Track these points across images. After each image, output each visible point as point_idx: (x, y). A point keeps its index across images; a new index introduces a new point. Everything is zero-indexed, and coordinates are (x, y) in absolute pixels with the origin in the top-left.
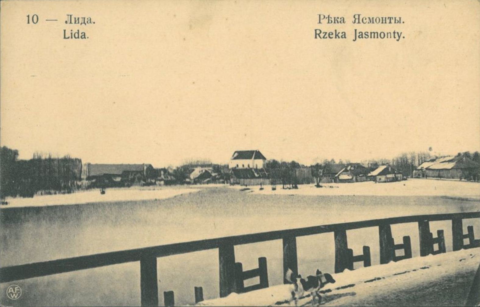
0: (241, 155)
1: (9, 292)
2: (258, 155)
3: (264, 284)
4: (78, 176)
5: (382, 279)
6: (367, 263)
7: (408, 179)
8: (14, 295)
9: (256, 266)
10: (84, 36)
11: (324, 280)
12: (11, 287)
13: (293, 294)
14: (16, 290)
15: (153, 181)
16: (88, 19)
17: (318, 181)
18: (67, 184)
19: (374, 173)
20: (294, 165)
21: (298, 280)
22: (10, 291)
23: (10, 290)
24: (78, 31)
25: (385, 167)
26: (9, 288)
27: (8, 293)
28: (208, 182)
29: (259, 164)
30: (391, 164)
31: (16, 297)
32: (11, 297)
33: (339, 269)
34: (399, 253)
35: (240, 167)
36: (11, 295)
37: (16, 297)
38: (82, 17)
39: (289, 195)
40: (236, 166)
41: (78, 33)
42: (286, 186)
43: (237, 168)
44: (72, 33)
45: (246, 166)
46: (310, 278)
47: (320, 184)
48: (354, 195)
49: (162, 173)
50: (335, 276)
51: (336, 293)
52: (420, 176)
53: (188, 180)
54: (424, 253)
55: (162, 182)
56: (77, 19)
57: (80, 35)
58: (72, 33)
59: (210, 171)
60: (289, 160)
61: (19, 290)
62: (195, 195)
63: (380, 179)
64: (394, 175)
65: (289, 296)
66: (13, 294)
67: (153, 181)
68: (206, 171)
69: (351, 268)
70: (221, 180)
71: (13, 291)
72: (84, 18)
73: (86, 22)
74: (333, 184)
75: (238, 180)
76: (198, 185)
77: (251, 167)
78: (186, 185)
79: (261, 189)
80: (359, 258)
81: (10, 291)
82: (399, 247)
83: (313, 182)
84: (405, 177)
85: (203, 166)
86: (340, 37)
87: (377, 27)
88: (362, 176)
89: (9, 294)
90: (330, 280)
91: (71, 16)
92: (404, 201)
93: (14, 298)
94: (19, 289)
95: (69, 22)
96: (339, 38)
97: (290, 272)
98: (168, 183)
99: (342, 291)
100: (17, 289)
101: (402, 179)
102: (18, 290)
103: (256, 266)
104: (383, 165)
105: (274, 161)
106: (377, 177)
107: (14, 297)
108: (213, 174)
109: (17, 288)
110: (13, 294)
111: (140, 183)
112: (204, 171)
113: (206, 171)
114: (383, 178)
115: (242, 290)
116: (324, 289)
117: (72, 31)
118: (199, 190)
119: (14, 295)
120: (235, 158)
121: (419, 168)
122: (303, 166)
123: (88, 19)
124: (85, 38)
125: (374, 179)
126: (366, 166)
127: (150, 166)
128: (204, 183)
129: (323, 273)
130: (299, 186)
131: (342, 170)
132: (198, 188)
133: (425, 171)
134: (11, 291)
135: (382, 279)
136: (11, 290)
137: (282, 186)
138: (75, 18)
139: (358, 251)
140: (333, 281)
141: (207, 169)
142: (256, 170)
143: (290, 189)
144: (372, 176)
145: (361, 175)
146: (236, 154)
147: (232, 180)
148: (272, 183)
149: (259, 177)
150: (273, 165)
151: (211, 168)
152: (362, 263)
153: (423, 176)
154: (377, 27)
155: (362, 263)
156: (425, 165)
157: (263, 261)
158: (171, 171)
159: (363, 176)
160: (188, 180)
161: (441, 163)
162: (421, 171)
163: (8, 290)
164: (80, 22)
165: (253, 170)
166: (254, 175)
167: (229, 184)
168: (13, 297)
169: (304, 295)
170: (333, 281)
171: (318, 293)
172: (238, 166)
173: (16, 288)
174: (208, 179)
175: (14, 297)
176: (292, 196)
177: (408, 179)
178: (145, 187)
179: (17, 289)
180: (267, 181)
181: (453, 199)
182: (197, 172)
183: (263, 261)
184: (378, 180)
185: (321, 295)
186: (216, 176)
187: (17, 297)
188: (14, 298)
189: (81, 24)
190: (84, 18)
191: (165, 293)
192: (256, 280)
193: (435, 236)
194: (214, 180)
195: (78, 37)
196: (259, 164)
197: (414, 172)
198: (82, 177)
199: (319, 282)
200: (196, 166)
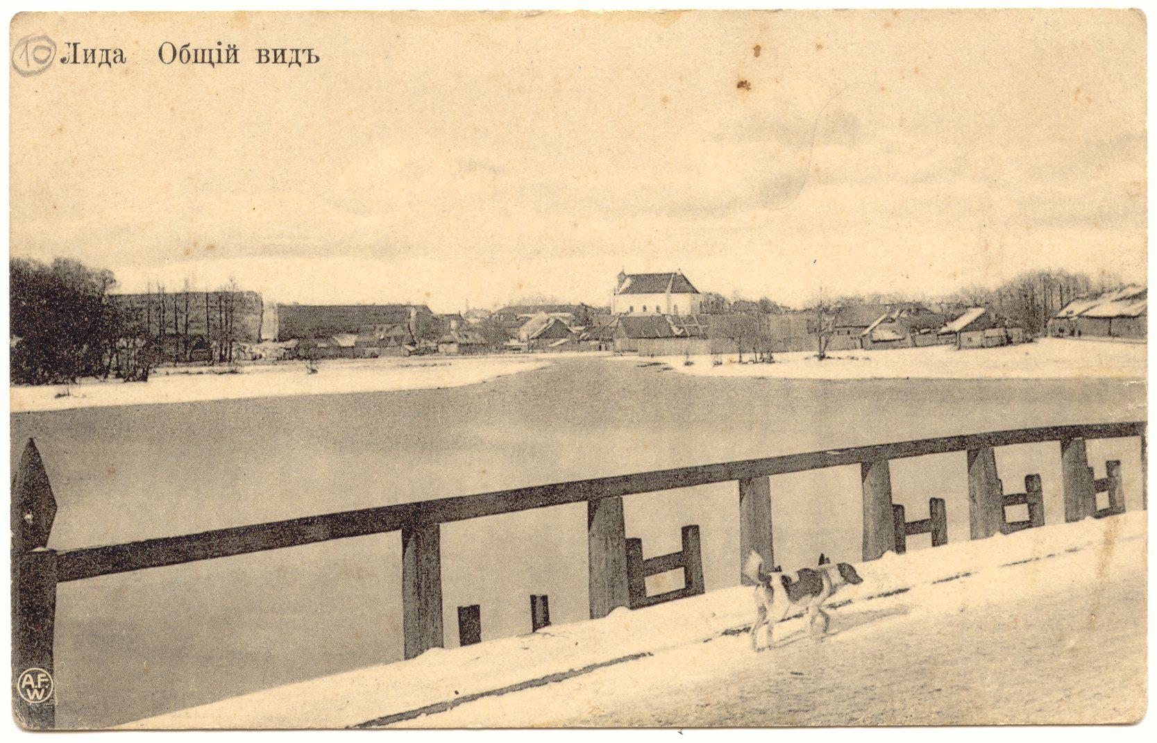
0: (643, 283)
1: (23, 686)
2: (680, 284)
3: (692, 588)
4: (254, 332)
6: (939, 540)
7: (1035, 340)
8: (36, 692)
9: (675, 546)
11: (836, 577)
12: (28, 673)
13: (763, 610)
14: (40, 680)
15: (432, 345)
17: (823, 346)
18: (228, 355)
19: (957, 325)
20: (766, 307)
21: (776, 580)
22: (25, 683)
23: (25, 679)
25: (980, 311)
26: (24, 676)
27: (21, 688)
28: (562, 348)
29: (683, 304)
30: (996, 304)
31: (39, 697)
32: (27, 697)
33: (871, 552)
34: (1017, 513)
35: (638, 311)
36: (28, 691)
37: (39, 697)
38: (103, 48)
39: (755, 378)
40: (629, 310)
42: (746, 357)
43: (631, 315)
45: (652, 311)
46: (803, 572)
47: (828, 354)
48: (908, 378)
49: (454, 324)
50: (861, 568)
51: (865, 609)
52: (1065, 334)
53: (514, 343)
54: (1072, 517)
55: (454, 348)
56: (89, 52)
59: (565, 322)
60: (753, 294)
61: (46, 680)
63: (970, 340)
64: (1002, 329)
65: (751, 617)
67: (432, 345)
68: (557, 321)
69: (900, 548)
70: (593, 343)
71: (32, 683)
72: (107, 51)
73: (111, 60)
74: (859, 353)
75: (633, 343)
76: (539, 355)
77: (663, 311)
78: (508, 354)
79: (687, 364)
80: (917, 527)
81: (25, 683)
82: (1014, 499)
83: (810, 348)
84: (1029, 336)
85: (550, 309)
88: (924, 333)
89: (24, 691)
90: (850, 575)
91: (75, 45)
92: (1033, 391)
93: (36, 699)
94: (47, 677)
95: (72, 60)
97: (755, 560)
98: (467, 349)
99: (876, 605)
100: (42, 678)
101: (1021, 339)
102: (43, 680)
103: (675, 546)
104: (977, 306)
105: (717, 297)
106: (962, 334)
108: (574, 330)
109: (44, 675)
110: (32, 690)
112: (552, 321)
113: (557, 321)
114: (977, 337)
115: (638, 599)
116: (836, 599)
118: (539, 365)
120: (626, 291)
121: (1063, 313)
122: (787, 310)
123: (115, 52)
125: (954, 338)
126: (937, 310)
127: (425, 308)
128: (553, 349)
129: (835, 559)
130: (776, 356)
131: (880, 320)
132: (538, 360)
133: (1075, 321)
134: (28, 683)
136: (28, 679)
137: (736, 357)
138: (86, 51)
139: (917, 511)
140: (857, 580)
141: (558, 315)
142: (677, 319)
143: (755, 362)
144: (950, 333)
145: (922, 331)
146: (628, 282)
147: (618, 343)
148: (714, 352)
149: (683, 336)
150: (715, 306)
151: (567, 315)
152: (928, 536)
153: (1072, 333)
155: (928, 536)
156: (1077, 308)
157: (690, 533)
158: (472, 321)
159: (929, 332)
160: (514, 343)
161: (1115, 304)
162: (1066, 320)
163: (22, 681)
164: (98, 60)
165: (668, 319)
166: (671, 331)
167: (610, 353)
168: (32, 697)
169: (791, 614)
170: (857, 580)
171: (822, 608)
172: (631, 308)
173: (39, 676)
174: (563, 341)
176: (762, 381)
177: (1035, 340)
178: (414, 360)
179: (42, 678)
180: (702, 345)
182: (537, 322)
183: (690, 533)
184: (965, 342)
185: (830, 612)
186: (581, 332)
187: (45, 696)
188: (36, 699)
189: (100, 64)
190: (107, 51)
191: (460, 609)
192: (673, 579)
193: (1101, 473)
194: (577, 343)
196: (683, 304)
197: (1050, 322)
198: (263, 337)
199: (825, 582)
200: (536, 309)
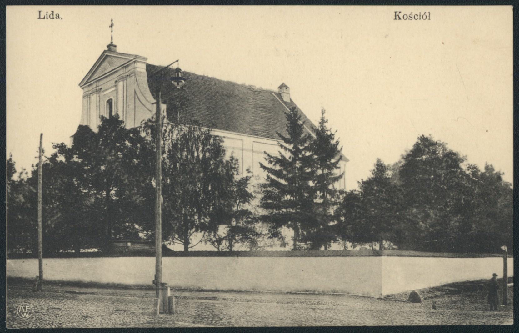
1: (20, 312)
5: (12, 157)
8: (25, 314)
10: (58, 17)
16: (56, 15)
24: (53, 12)
36: (22, 314)
41: (53, 14)
44: (47, 15)
57: (55, 16)
58: (47, 15)
62: (452, 290)
66: (23, 313)
81: (20, 310)
86: (401, 17)
87: (125, 115)
93: (25, 317)
96: (400, 19)
107: (25, 316)
111: (261, 207)
117: (47, 12)
119: (25, 314)
124: (59, 18)
135: (12, 157)
154: (125, 115)
163: (19, 310)
175: (25, 316)
181: (352, 256)
195: (53, 18)
